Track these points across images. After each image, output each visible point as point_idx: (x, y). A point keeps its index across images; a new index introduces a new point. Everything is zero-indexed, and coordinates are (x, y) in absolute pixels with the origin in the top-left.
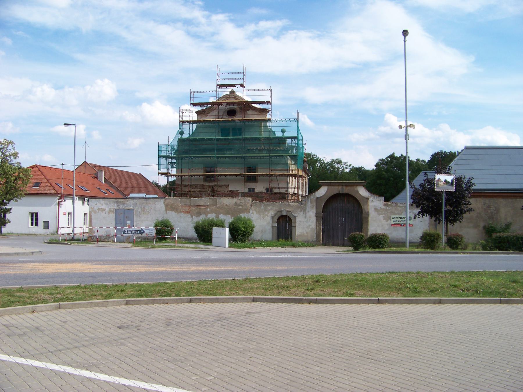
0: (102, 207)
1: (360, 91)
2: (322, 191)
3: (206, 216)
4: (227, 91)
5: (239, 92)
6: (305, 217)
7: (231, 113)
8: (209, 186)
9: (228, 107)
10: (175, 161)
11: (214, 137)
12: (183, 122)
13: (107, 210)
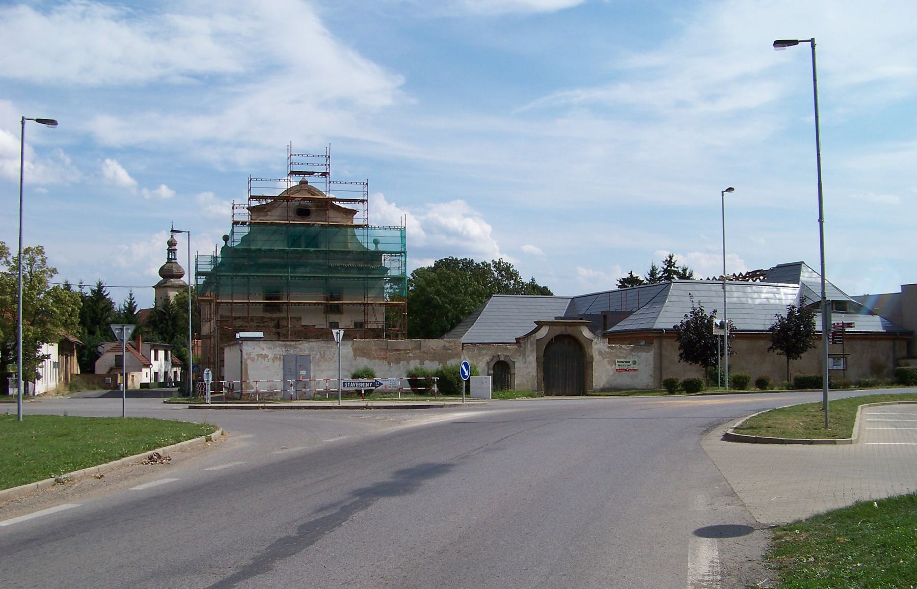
0: (264, 353)
1: (200, 127)
3: (422, 363)
5: (312, 181)
7: (303, 212)
8: (272, 319)
9: (302, 203)
12: (235, 223)
13: (271, 356)
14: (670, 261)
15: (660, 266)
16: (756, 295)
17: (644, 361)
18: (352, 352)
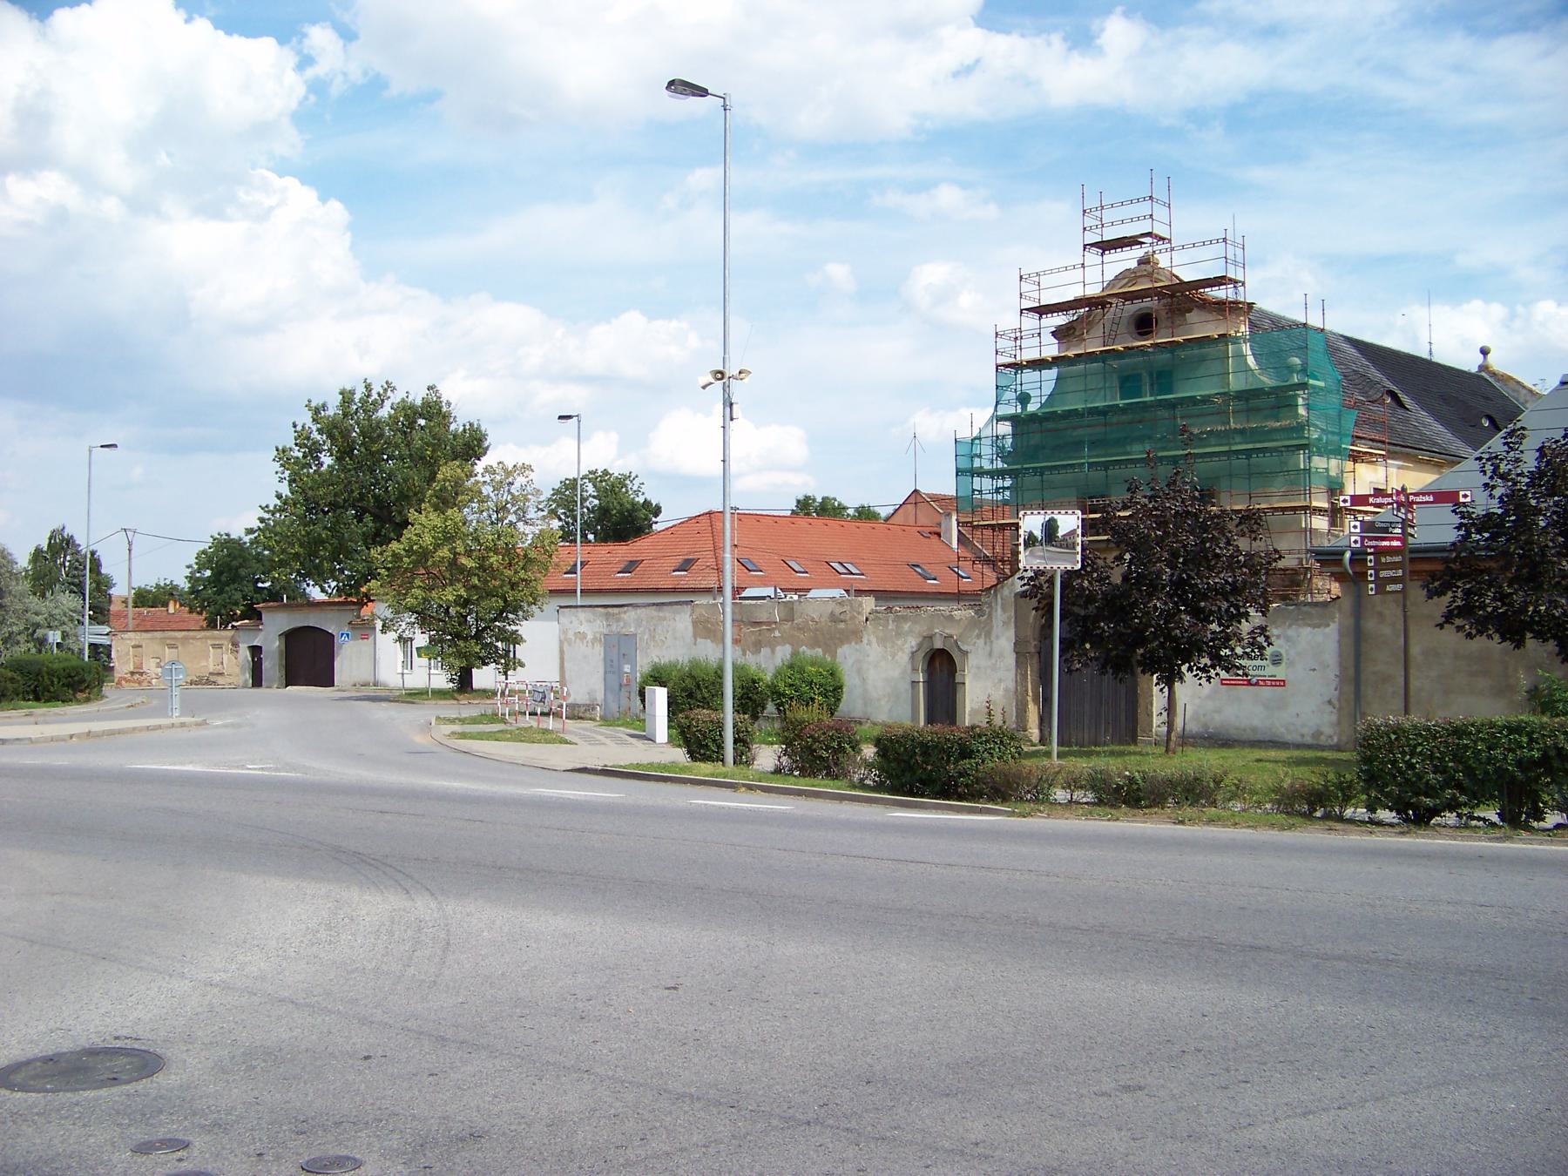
4: (1127, 259)
6: (990, 654)
7: (1144, 324)
10: (1008, 483)
11: (1080, 407)
12: (1017, 367)
13: (590, 637)
18: (690, 627)
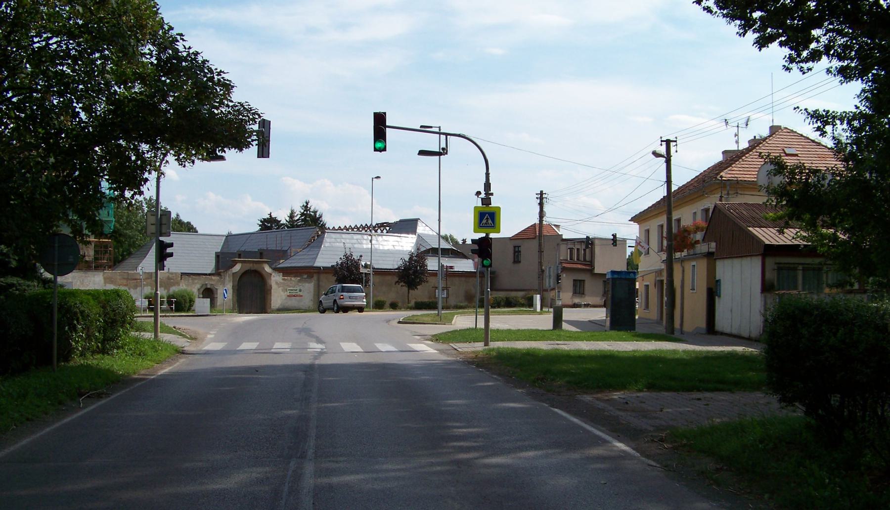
2: (237, 268)
14: (306, 207)
15: (298, 210)
16: (385, 243)
17: (307, 289)
